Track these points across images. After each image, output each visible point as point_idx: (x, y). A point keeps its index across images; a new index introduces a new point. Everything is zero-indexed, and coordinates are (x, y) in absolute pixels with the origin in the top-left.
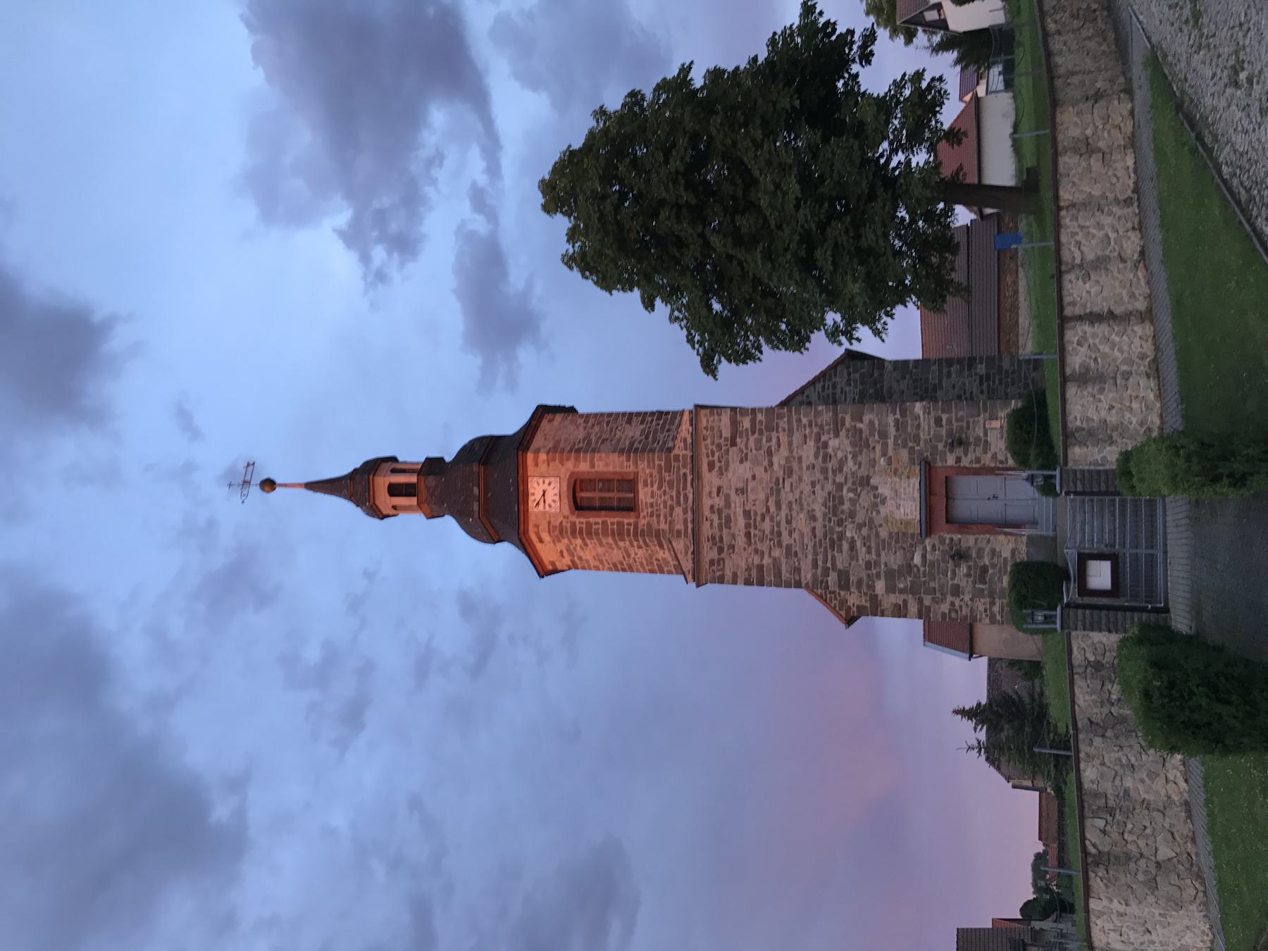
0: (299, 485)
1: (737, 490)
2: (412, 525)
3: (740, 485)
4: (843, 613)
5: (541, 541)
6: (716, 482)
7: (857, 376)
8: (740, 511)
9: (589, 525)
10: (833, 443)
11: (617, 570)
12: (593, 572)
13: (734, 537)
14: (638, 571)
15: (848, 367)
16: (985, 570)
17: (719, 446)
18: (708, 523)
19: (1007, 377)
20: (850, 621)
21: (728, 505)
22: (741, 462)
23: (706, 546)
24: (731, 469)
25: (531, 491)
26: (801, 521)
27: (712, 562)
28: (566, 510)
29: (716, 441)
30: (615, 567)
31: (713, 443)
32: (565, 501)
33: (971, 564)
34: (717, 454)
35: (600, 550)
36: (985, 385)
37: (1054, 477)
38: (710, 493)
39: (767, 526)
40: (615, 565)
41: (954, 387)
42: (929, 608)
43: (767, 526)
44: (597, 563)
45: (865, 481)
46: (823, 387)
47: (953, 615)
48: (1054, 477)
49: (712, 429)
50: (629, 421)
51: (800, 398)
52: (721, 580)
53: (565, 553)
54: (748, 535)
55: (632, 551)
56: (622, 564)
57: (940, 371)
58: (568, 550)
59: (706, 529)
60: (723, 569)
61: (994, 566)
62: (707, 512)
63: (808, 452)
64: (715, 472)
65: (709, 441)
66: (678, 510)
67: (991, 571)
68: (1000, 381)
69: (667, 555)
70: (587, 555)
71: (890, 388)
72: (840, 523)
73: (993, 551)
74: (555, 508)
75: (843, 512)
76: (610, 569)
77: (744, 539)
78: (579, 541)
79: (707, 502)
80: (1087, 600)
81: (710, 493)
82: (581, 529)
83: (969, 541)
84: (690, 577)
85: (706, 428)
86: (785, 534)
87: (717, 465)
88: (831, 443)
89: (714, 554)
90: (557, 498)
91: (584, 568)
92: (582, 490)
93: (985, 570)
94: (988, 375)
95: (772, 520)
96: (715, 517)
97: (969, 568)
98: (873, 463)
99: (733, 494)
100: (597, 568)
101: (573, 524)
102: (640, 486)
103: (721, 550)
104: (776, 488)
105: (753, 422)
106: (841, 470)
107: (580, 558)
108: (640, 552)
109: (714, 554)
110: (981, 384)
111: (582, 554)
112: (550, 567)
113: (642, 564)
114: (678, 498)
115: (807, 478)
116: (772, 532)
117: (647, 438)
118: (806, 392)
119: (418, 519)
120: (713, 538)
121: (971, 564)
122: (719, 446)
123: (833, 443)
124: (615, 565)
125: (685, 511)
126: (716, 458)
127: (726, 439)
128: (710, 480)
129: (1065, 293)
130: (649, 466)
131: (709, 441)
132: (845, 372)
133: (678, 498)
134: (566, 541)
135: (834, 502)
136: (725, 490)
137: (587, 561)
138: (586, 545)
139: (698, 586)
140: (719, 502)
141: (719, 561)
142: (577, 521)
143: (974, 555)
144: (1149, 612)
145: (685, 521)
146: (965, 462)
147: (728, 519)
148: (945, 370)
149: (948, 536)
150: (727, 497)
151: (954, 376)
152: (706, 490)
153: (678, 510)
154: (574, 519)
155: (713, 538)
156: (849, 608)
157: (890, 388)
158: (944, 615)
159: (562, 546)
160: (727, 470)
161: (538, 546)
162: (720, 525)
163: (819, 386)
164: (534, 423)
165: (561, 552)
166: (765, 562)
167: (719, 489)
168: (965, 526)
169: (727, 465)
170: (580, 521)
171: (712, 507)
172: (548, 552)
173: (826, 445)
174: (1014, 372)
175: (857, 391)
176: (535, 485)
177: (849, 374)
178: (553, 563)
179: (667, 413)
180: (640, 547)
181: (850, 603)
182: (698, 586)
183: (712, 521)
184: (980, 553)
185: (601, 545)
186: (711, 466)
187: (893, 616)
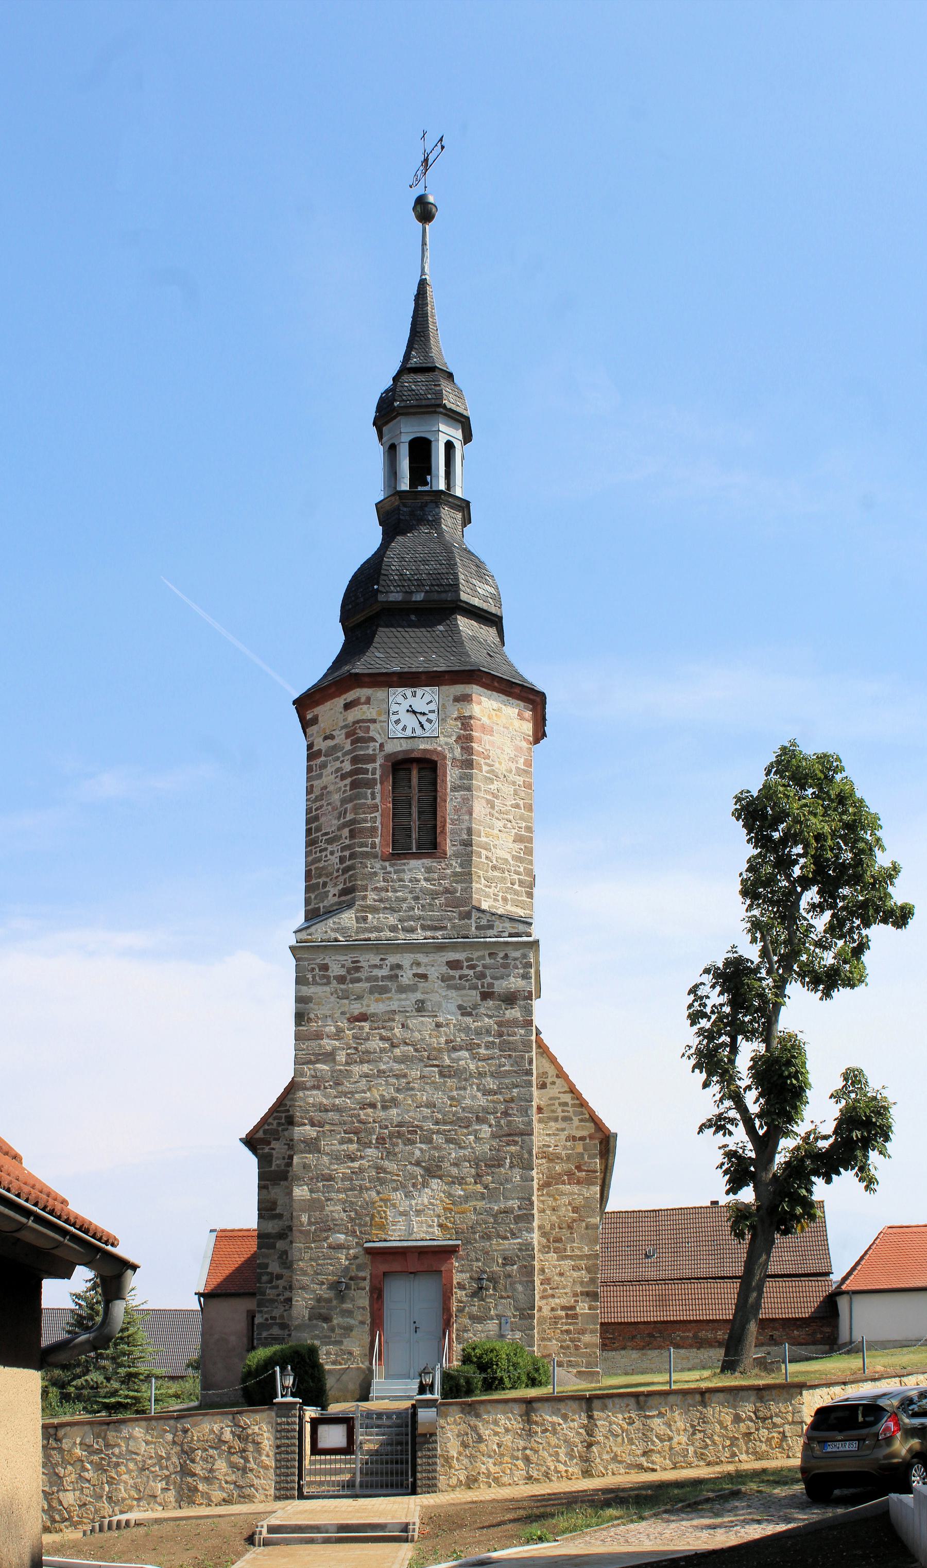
0: (423, 273)
1: (423, 1002)
2: (363, 474)
3: (428, 1006)
4: (260, 1134)
5: (348, 706)
6: (433, 973)
7: (580, 1149)
8: (395, 1006)
9: (370, 784)
10: (485, 1131)
11: (308, 822)
12: (304, 784)
13: (359, 998)
14: (308, 854)
15: (591, 1137)
16: (327, 1319)
17: (482, 976)
18: (378, 962)
19: (571, 1340)
20: (251, 1142)
21: (402, 989)
22: (460, 1007)
23: (347, 959)
24: (453, 993)
25: (419, 691)
26: (382, 1090)
27: (325, 968)
28: (390, 748)
29: (488, 972)
30: (312, 819)
31: (484, 966)
32: (405, 746)
33: (335, 1303)
34: (471, 972)
35: (336, 797)
36: (563, 1313)
37: (432, 1392)
38: (418, 964)
39: (375, 1044)
40: (316, 818)
41: (561, 1274)
42: (273, 1246)
43: (375, 1044)
44: (317, 792)
45: (432, 1171)
46: (566, 1104)
47: (265, 1278)
48: (432, 1392)
49: (506, 966)
50: (519, 839)
51: (552, 1071)
52: (300, 981)
53: (330, 743)
54: (363, 1017)
55: (334, 847)
56: (318, 829)
57: (581, 1258)
58: (335, 748)
59: (368, 959)
60: (315, 983)
61: (332, 1330)
62: (393, 959)
63: (474, 1098)
64: (444, 969)
65: (488, 961)
66: (392, 920)
67: (325, 1325)
68: (568, 1332)
69: (331, 900)
70: (328, 778)
71: (562, 1194)
72: (381, 1140)
73: (349, 1329)
74: (396, 731)
75: (395, 1145)
76: (309, 811)
77: (356, 1012)
78: (347, 767)
79: (406, 960)
80: (308, 1427)
81: (418, 964)
82: (366, 771)
83: (362, 1300)
84: (303, 936)
85: (506, 956)
86: (366, 1068)
87: (457, 974)
88: (485, 1128)
89: (336, 970)
90: (409, 733)
91: (309, 769)
92: (420, 770)
93: (327, 1319)
94: (575, 1316)
95: (383, 1050)
96: (385, 972)
97: (329, 1301)
98: (461, 1181)
99: (419, 996)
100: (310, 790)
101: (372, 759)
102: (427, 862)
103: (341, 980)
104: (430, 1057)
105: (514, 1023)
106: (449, 1141)
107: (324, 766)
108: (335, 859)
109: (336, 970)
110: (564, 1308)
111: (330, 769)
112: (309, 716)
113: (319, 860)
114: (411, 918)
115: (439, 1097)
116: (367, 1052)
117: (494, 868)
118: (559, 1081)
119: (375, 490)
120: (358, 969)
121: (335, 1303)
122: (482, 976)
123: (485, 1131)
124: (316, 818)
125: (393, 929)
126: (466, 972)
127: (491, 985)
128: (435, 966)
129: (617, 1400)
130: (455, 874)
131: (488, 961)
132: (585, 1133)
133: (411, 918)
134: (348, 747)
135: (405, 1133)
136: (422, 985)
137: (320, 776)
138: (343, 777)
139: (292, 948)
140: (406, 977)
141: (328, 977)
142: (377, 765)
143: (345, 1306)
144: (299, 1483)
145: (378, 929)
146: (459, 1294)
147: (384, 990)
148: (582, 1263)
149: (365, 1274)
150: (412, 989)
151: (575, 1274)
152: (421, 958)
153: (392, 920)
154: (379, 761)
155: (358, 969)
156: (269, 1143)
157: (562, 1194)
158: (266, 1266)
159: (340, 737)
160: (449, 987)
161: (340, 701)
162: (376, 979)
163: (567, 1098)
164: (517, 690)
165: (331, 737)
166: (325, 1041)
167: (424, 977)
168: (377, 1295)
169: (457, 988)
170: (376, 769)
171: (399, 967)
172: (330, 713)
173: (479, 1120)
174: (577, 1348)
175: (559, 1150)
176: (427, 698)
177: (582, 1139)
178: (315, 721)
179: (530, 895)
180: (342, 860)
181: (274, 1144)
182: (292, 948)
183: (381, 967)
184: (349, 1313)
185: (344, 801)
186: (454, 965)
187: (260, 1202)
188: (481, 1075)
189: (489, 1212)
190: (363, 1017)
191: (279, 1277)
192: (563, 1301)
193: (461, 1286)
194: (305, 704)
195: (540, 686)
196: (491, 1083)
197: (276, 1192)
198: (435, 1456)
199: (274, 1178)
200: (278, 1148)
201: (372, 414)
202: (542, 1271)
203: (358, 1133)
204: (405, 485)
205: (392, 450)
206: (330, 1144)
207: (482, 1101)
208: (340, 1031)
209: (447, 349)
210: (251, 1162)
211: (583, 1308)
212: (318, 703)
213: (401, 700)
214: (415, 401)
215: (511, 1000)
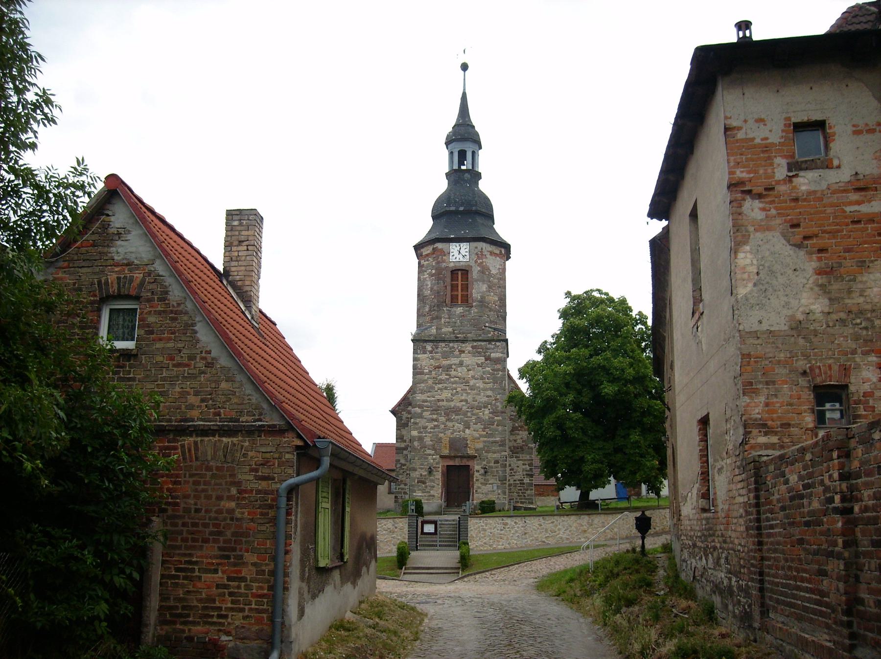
16: (424, 483)
20: (394, 412)
26: (446, 394)
61: (426, 487)
74: (452, 259)
86: (440, 386)
105: (498, 370)
123: (487, 412)
148: (527, 462)
172: (427, 251)
184: (433, 481)
188: (486, 390)
189: (488, 442)
190: (439, 367)
191: (405, 465)
192: (519, 478)
193: (478, 471)
194: (418, 248)
195: (509, 242)
196: (489, 393)
197: (404, 432)
198: (99, 282)
199: (401, 425)
200: (405, 415)
201: (444, 140)
202: (510, 465)
203: (436, 410)
204: (456, 167)
205: (451, 153)
206: (426, 414)
207: (486, 399)
208: (430, 371)
209: (476, 118)
210: (393, 419)
211: (527, 480)
212: (423, 247)
213: (454, 248)
214: (464, 138)
215: (757, 469)
